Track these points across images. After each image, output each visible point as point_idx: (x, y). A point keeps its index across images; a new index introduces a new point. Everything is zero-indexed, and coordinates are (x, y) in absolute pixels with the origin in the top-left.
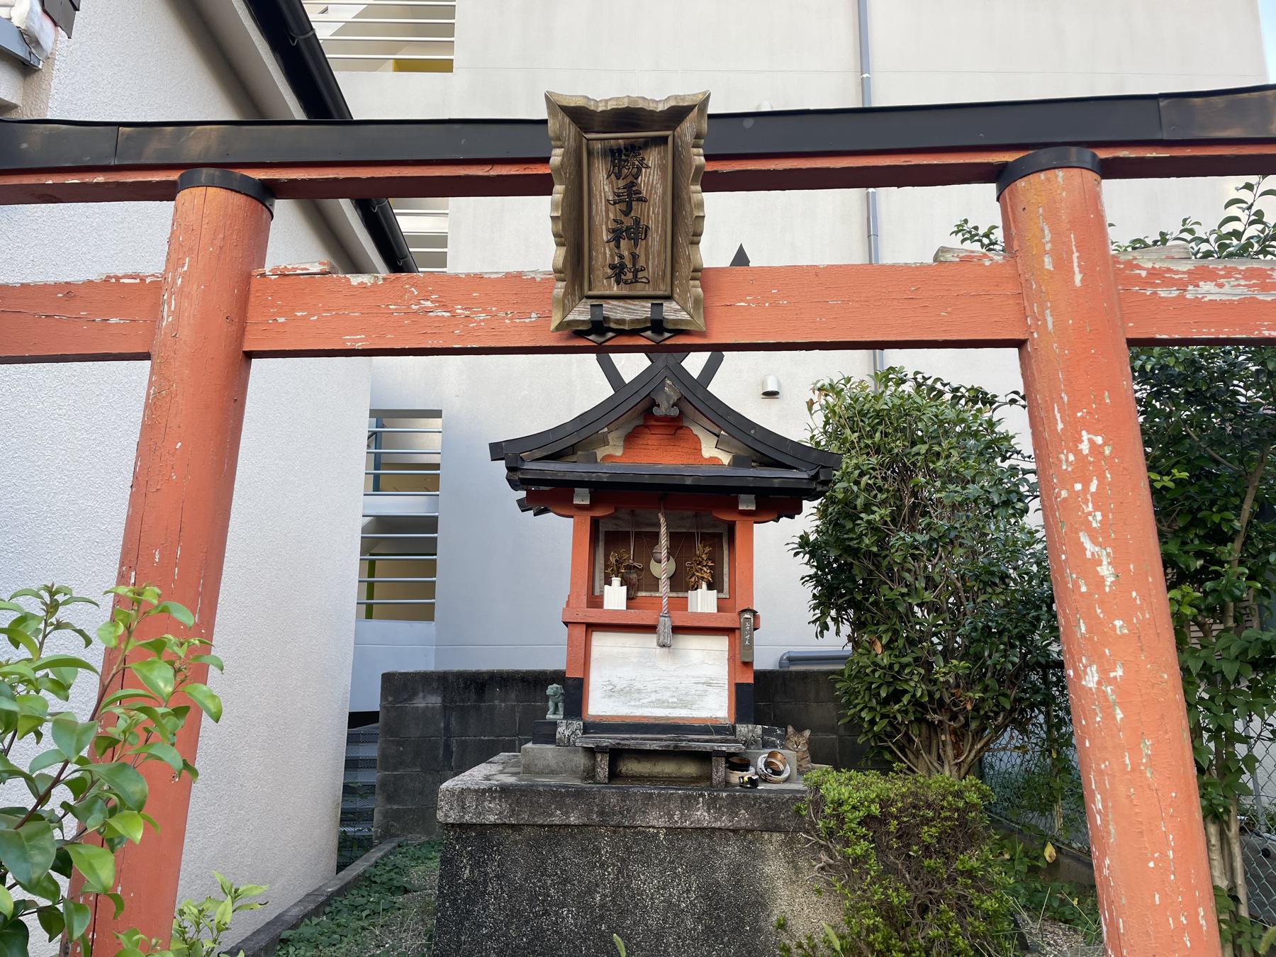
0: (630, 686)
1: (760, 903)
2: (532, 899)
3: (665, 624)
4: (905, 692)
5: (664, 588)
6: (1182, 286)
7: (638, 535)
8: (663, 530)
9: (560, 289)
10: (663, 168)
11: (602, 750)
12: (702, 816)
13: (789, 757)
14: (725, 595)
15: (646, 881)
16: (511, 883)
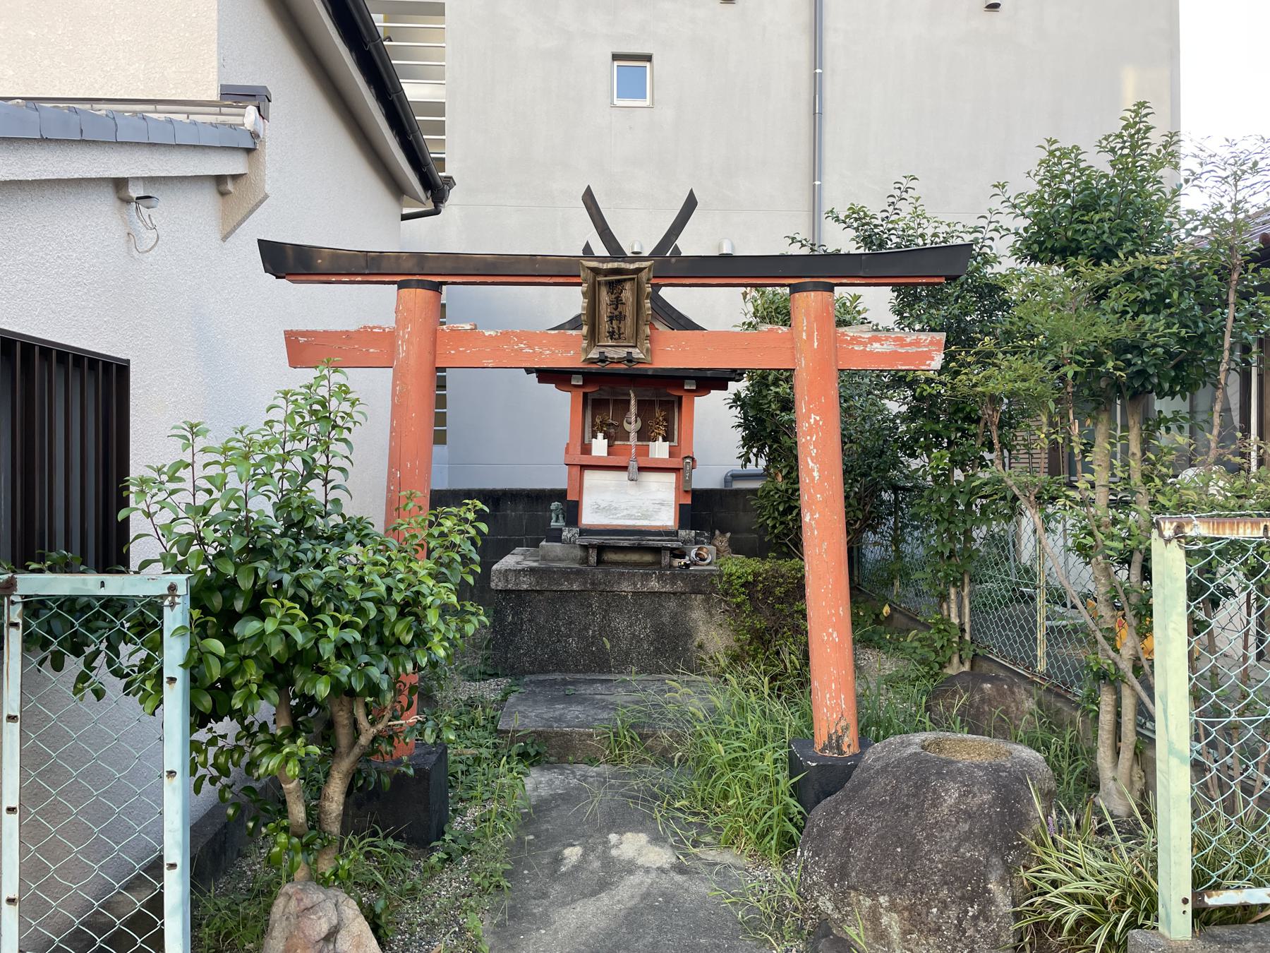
1: (689, 634)
2: (550, 633)
3: (633, 466)
5: (633, 440)
6: (865, 345)
7: (615, 401)
9: (585, 343)
10: (632, 290)
11: (593, 546)
12: (654, 585)
13: (709, 552)
14: (675, 443)
15: (620, 622)
16: (537, 624)
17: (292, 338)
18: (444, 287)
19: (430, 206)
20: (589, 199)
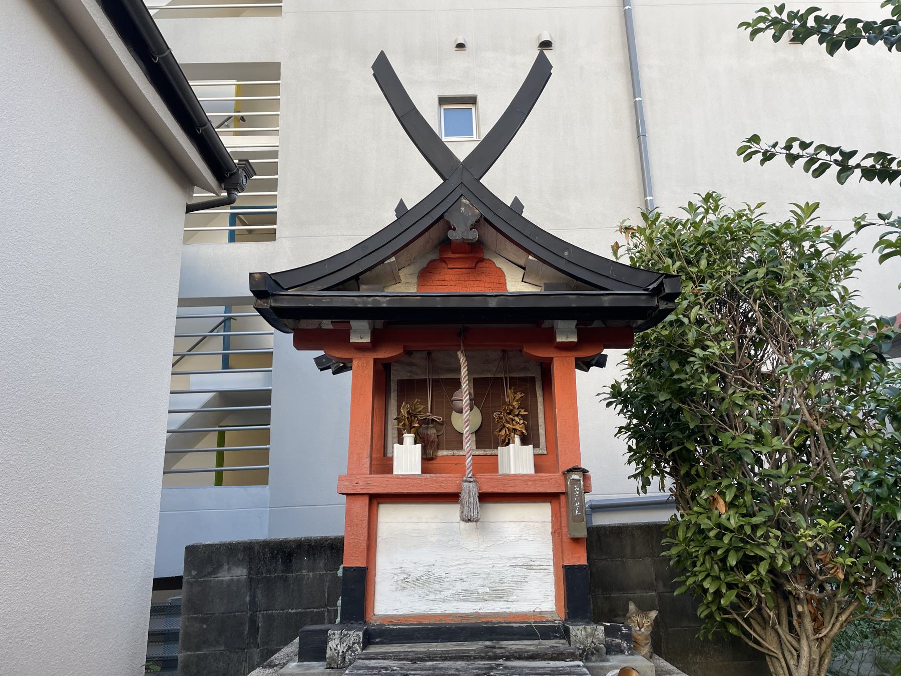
0: (429, 574)
3: (470, 491)
4: (759, 559)
5: (469, 444)
7: (436, 382)
8: (464, 371)
14: (542, 450)
20: (383, 72)
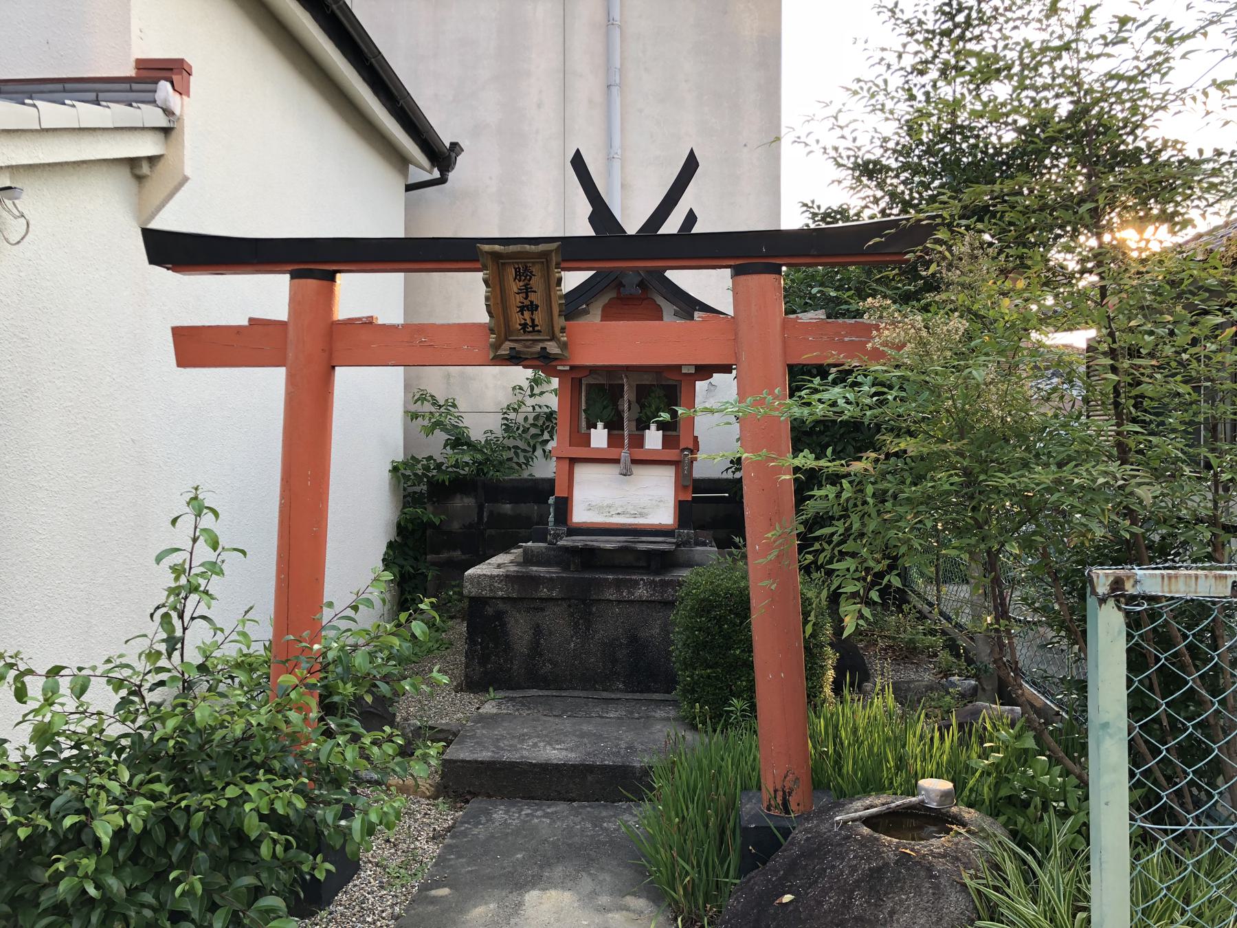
17: (180, 334)
18: (338, 275)
19: (436, 174)
